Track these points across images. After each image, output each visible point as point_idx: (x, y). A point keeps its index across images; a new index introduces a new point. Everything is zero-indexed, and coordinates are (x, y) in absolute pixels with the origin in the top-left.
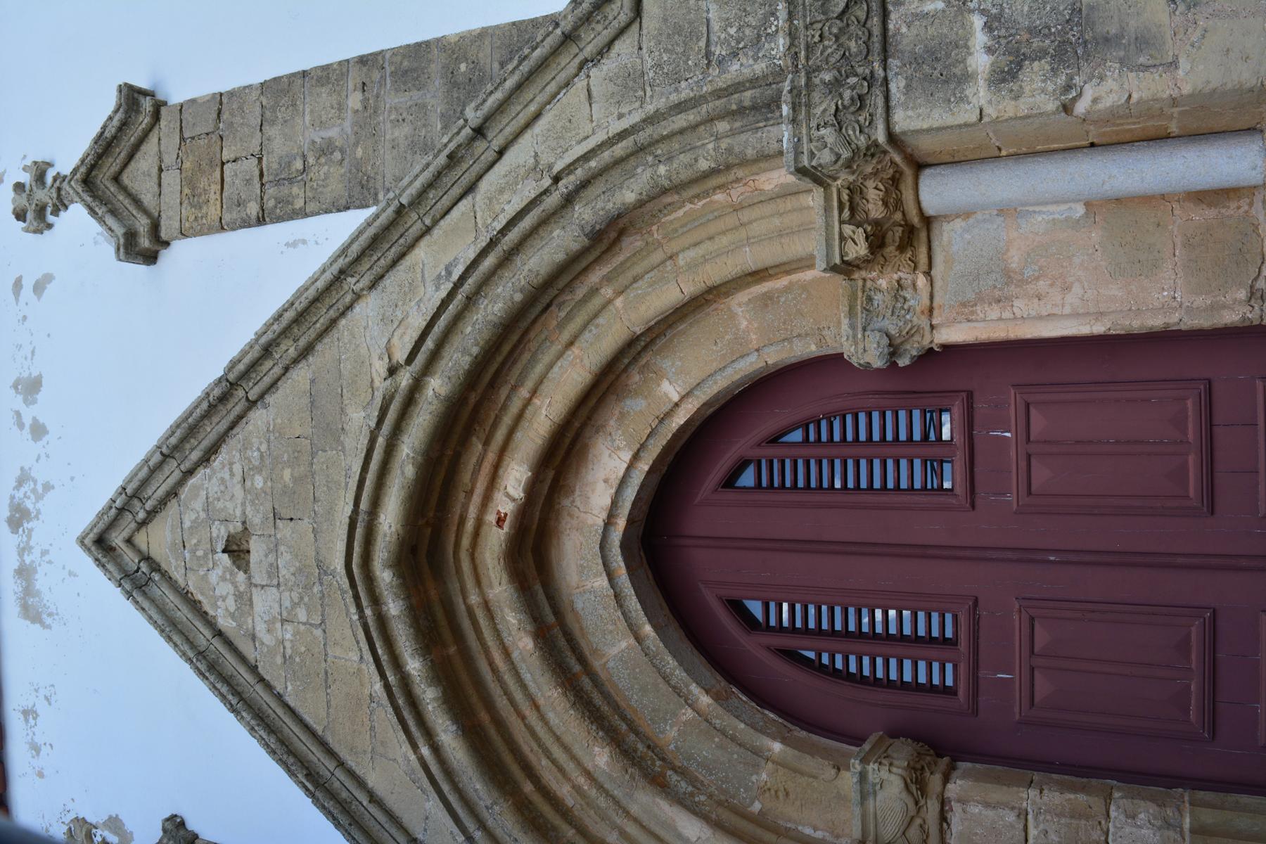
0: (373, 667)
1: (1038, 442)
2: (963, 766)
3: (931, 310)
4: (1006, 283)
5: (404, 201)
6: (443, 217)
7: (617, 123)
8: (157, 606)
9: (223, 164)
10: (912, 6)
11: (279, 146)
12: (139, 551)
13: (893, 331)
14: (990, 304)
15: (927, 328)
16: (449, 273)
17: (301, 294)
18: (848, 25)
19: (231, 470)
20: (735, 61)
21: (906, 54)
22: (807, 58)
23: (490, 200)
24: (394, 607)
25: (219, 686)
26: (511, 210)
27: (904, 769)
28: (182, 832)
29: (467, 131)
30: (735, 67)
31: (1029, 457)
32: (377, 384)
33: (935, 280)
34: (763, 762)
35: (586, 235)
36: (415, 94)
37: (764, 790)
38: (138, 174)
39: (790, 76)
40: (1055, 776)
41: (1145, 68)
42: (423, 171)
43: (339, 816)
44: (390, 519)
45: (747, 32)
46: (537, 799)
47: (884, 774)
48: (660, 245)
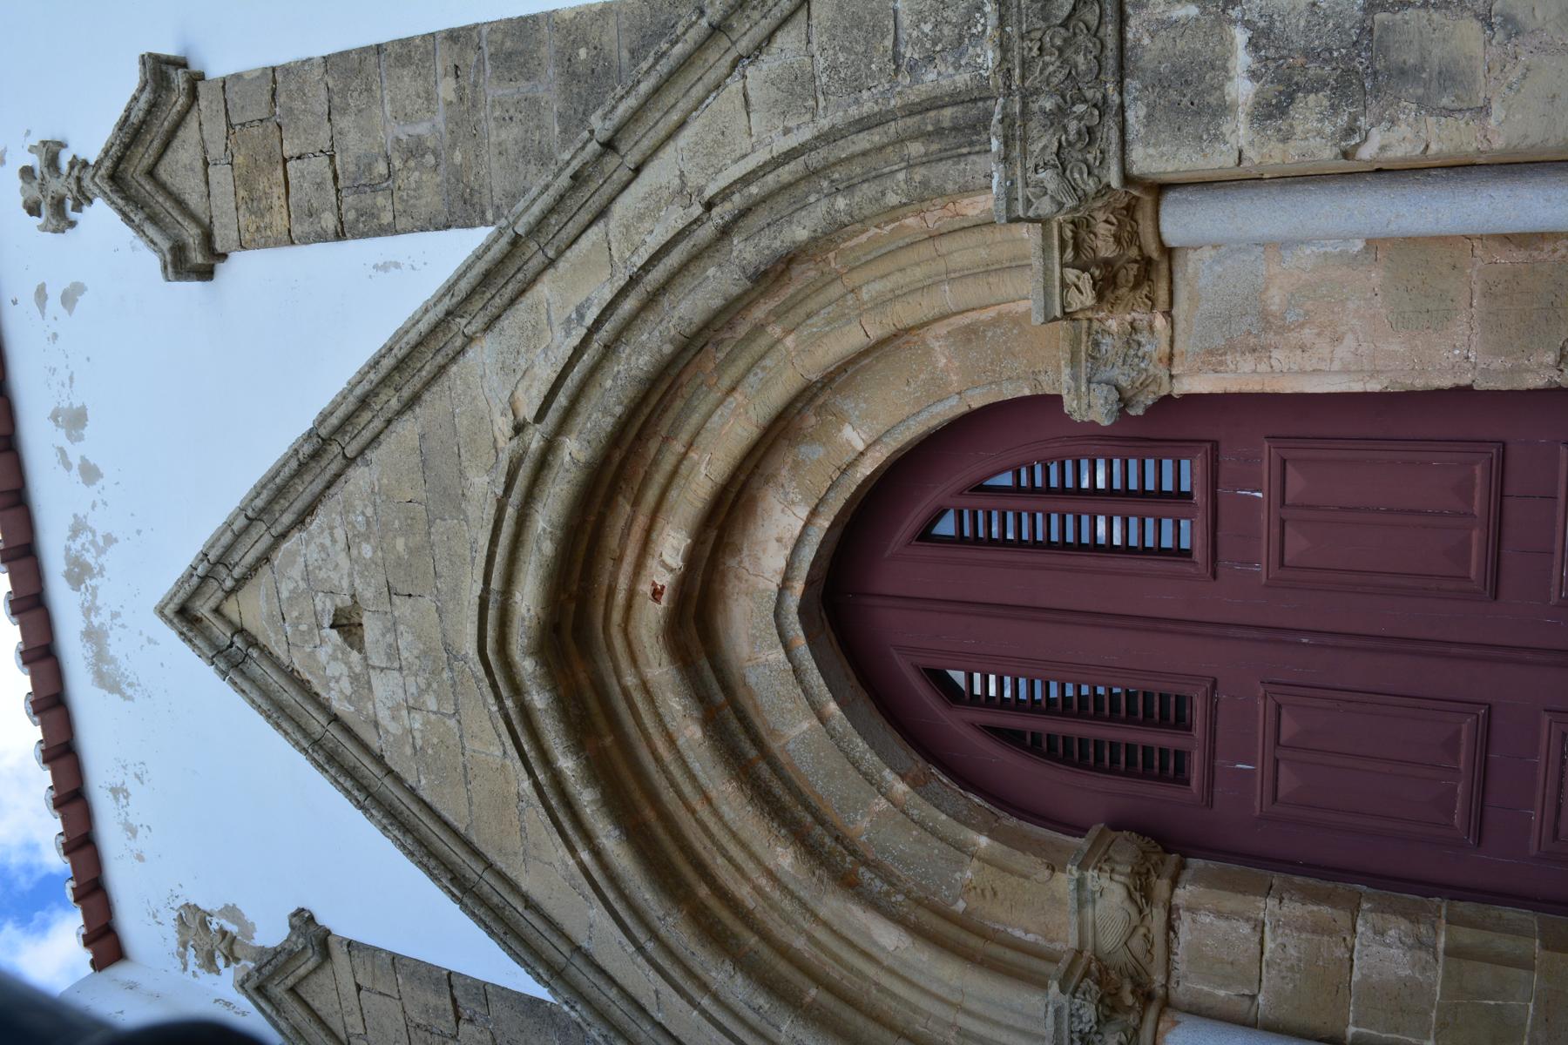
0: (519, 764)
1: (1294, 506)
2: (1195, 863)
3: (1171, 358)
4: (1263, 328)
5: (521, 230)
6: (569, 246)
7: (782, 139)
8: (259, 688)
9: (285, 161)
10: (1157, 7)
11: (354, 143)
12: (230, 623)
13: (1124, 382)
14: (1243, 353)
15: (1166, 379)
16: (581, 316)
17: (401, 338)
18: (1075, 34)
19: (332, 535)
20: (931, 67)
21: (1149, 74)
22: (1023, 78)
23: (627, 228)
24: (539, 700)
25: (341, 780)
26: (654, 242)
27: (1127, 875)
28: (312, 928)
29: (594, 147)
30: (931, 76)
31: (1283, 523)
32: (501, 444)
33: (1176, 320)
34: (967, 859)
35: (749, 278)
36: (524, 85)
37: (968, 889)
38: (178, 166)
39: (1001, 100)
40: (1298, 879)
41: (1449, 112)
42: (542, 193)
43: (492, 925)
44: (528, 599)
45: (946, 30)
46: (713, 903)
47: (1105, 881)
48: (839, 277)
